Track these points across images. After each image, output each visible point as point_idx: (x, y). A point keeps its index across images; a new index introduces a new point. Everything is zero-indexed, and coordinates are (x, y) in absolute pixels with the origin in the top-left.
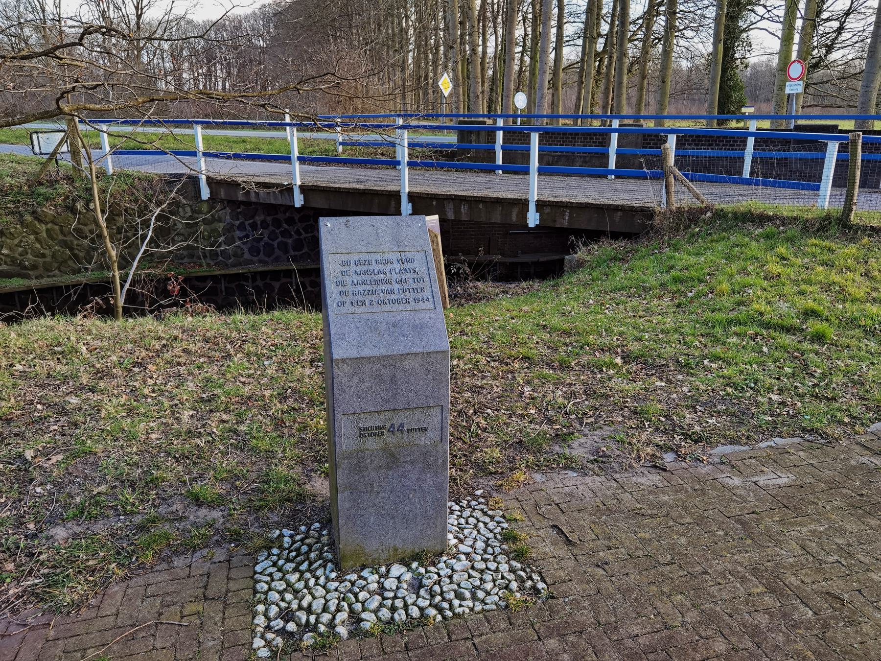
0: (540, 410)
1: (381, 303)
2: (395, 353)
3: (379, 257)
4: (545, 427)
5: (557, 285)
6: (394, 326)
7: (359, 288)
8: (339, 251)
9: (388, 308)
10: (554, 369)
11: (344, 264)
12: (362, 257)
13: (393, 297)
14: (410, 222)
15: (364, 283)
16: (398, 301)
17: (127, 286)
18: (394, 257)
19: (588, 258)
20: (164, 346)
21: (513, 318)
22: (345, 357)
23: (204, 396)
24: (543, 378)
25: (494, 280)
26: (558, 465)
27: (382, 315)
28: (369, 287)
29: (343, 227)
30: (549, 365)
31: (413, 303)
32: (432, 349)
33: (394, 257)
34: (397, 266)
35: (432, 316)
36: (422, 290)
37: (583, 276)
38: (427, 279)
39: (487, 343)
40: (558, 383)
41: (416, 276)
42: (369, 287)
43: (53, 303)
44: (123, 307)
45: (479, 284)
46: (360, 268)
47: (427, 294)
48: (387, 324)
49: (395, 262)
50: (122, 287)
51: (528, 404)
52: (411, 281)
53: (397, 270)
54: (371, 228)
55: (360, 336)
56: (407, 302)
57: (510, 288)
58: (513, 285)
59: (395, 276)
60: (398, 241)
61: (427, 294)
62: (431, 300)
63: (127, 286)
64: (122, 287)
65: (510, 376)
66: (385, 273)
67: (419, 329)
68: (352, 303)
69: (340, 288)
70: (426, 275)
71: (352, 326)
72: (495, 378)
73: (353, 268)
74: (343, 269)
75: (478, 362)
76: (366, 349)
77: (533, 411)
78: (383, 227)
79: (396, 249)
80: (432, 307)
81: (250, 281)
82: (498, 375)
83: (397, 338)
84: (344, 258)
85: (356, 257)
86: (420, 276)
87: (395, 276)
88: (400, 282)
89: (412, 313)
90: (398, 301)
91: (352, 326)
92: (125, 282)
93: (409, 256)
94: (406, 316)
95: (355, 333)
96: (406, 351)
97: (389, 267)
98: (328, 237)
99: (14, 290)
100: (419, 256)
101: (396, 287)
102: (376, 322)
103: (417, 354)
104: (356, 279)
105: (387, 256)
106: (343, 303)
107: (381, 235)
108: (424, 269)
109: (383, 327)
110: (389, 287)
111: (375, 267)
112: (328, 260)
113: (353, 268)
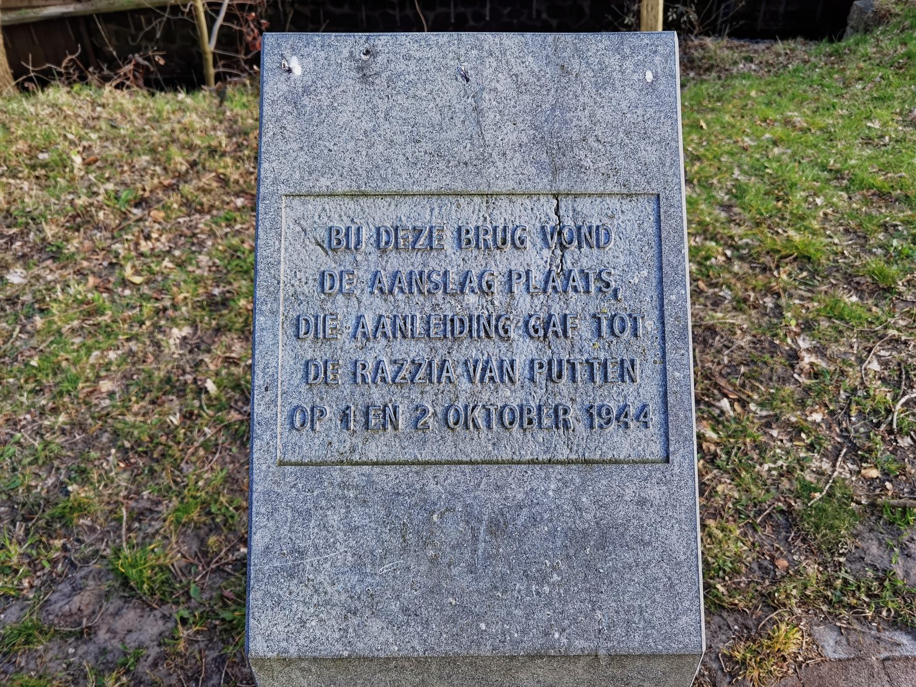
0: (832, 413)
1: (458, 420)
2: (486, 650)
3: (471, 214)
4: (844, 470)
5: (839, 55)
6: (497, 527)
7: (379, 350)
8: (324, 183)
9: (477, 445)
10: (860, 293)
11: (336, 241)
12: (406, 213)
13: (509, 396)
14: (613, 61)
15: (402, 329)
16: (524, 418)
17: (220, 21)
18: (530, 216)
19: (897, 10)
20: (193, 164)
21: (775, 143)
22: (293, 651)
23: (216, 291)
24: (835, 313)
25: (730, 36)
26: (878, 612)
27: (454, 475)
28: (416, 350)
29: (350, 80)
30: (851, 280)
31: (581, 428)
32: (635, 643)
33: (530, 216)
34: (536, 259)
35: (654, 493)
36: (626, 371)
37: (887, 43)
38: (649, 325)
39: (727, 207)
40: (872, 336)
41: (607, 307)
42: (416, 350)
43: (134, 40)
44: (214, 54)
45: (709, 41)
46: (395, 262)
47: (644, 390)
48: (469, 516)
49: (533, 240)
50: (211, 21)
51: (807, 390)
52: (585, 329)
53: (537, 277)
54: (453, 89)
55: (358, 568)
56: (560, 420)
57: (756, 51)
58: (761, 46)
59: (524, 303)
60: (554, 149)
61: (644, 390)
62: (655, 418)
63: (220, 21)
64: (211, 21)
65: (769, 302)
66: (486, 290)
67: (595, 544)
68: (345, 417)
69: (308, 350)
70: (648, 303)
71: (334, 518)
72: (741, 304)
73: (368, 261)
74: (328, 263)
75: (707, 258)
76: (375, 625)
77: (817, 417)
78: (504, 84)
79: (543, 183)
80: (655, 450)
81: (398, 9)
82: (745, 300)
83: (501, 583)
84: (338, 214)
85: (384, 214)
86: (623, 307)
87: (524, 303)
88: (544, 329)
89: (575, 475)
90: (524, 418)
91: (334, 518)
92: (218, 13)
93: (592, 212)
94: (548, 485)
95: (342, 555)
96: (533, 641)
97: (505, 261)
98: (289, 121)
99: (122, 8)
100: (630, 220)
101: (524, 350)
102: (427, 506)
103: (567, 657)
104: (373, 307)
105: (505, 214)
106: (314, 415)
107: (491, 117)
108: (643, 275)
109: (453, 530)
110: (493, 349)
111: (451, 260)
112: (275, 225)
113: (368, 261)
